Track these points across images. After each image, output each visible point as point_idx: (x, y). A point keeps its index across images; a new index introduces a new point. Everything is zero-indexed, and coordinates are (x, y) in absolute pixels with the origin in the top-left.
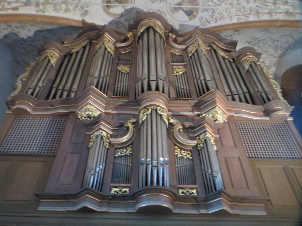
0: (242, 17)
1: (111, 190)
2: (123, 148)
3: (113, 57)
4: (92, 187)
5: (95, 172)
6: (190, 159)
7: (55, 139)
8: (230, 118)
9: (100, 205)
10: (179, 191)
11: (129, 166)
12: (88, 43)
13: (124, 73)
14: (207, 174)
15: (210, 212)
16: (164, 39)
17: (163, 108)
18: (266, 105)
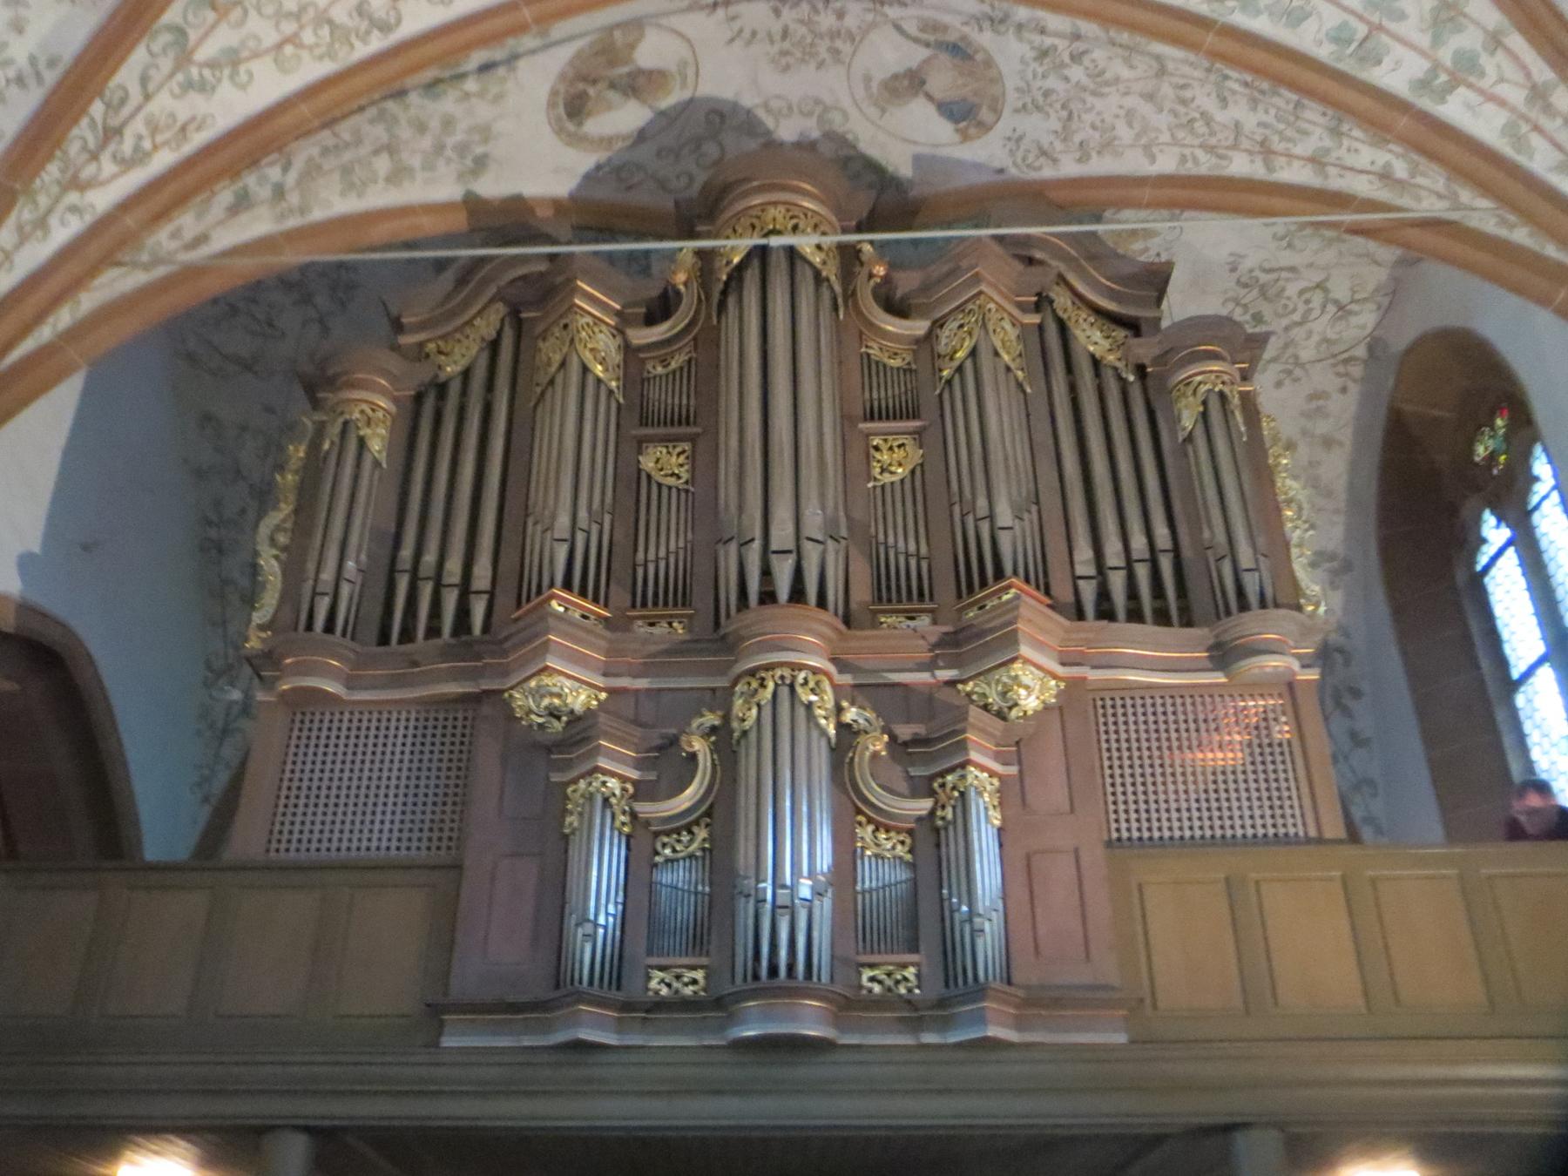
0: (1200, 153)
1: (649, 978)
2: (678, 831)
3: (619, 405)
4: (591, 983)
5: (596, 925)
6: (907, 863)
7: (447, 786)
8: (1074, 687)
9: (620, 1027)
10: (860, 974)
11: (703, 894)
12: (502, 320)
13: (670, 488)
14: (957, 916)
16: (838, 288)
17: (815, 671)
18: (1226, 622)
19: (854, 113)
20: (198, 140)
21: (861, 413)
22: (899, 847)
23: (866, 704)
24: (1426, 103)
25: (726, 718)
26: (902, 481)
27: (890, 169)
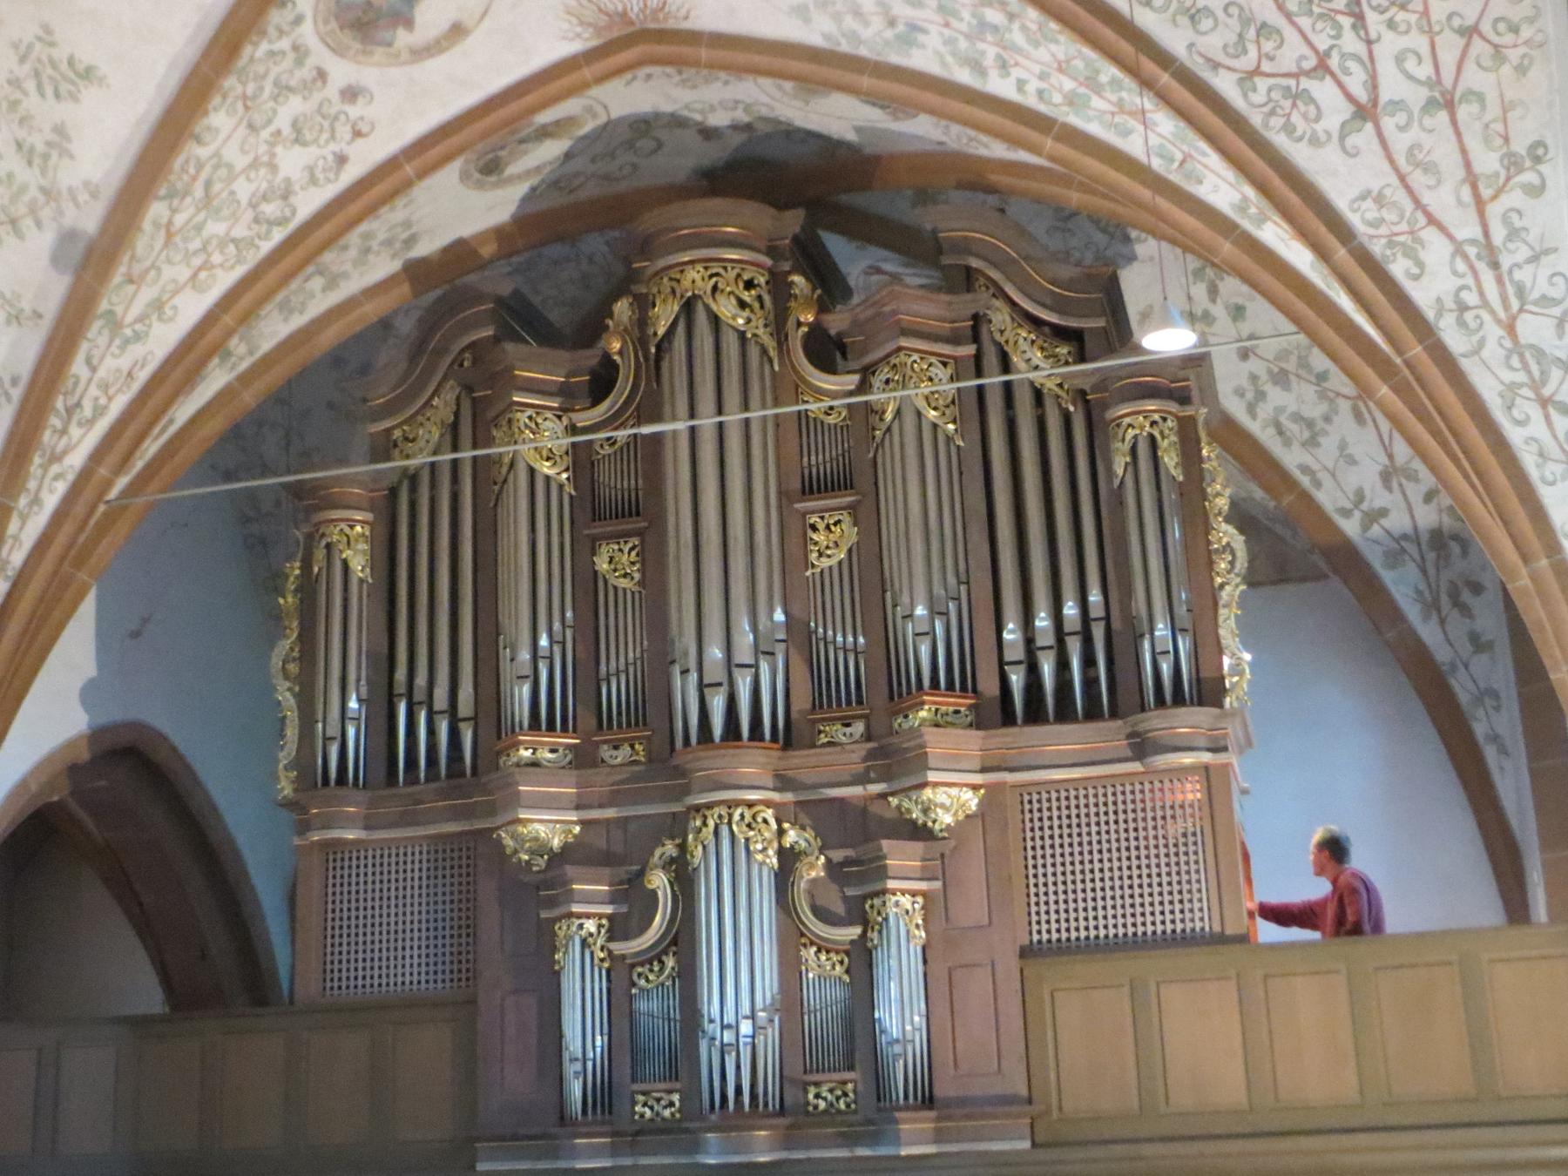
8: (992, 797)
15: (903, 1153)
19: (777, 105)
20: (143, 376)
21: (798, 486)
22: (838, 967)
23: (807, 821)
24: (1246, 225)
25: (683, 847)
26: (840, 563)
27: (835, 137)
